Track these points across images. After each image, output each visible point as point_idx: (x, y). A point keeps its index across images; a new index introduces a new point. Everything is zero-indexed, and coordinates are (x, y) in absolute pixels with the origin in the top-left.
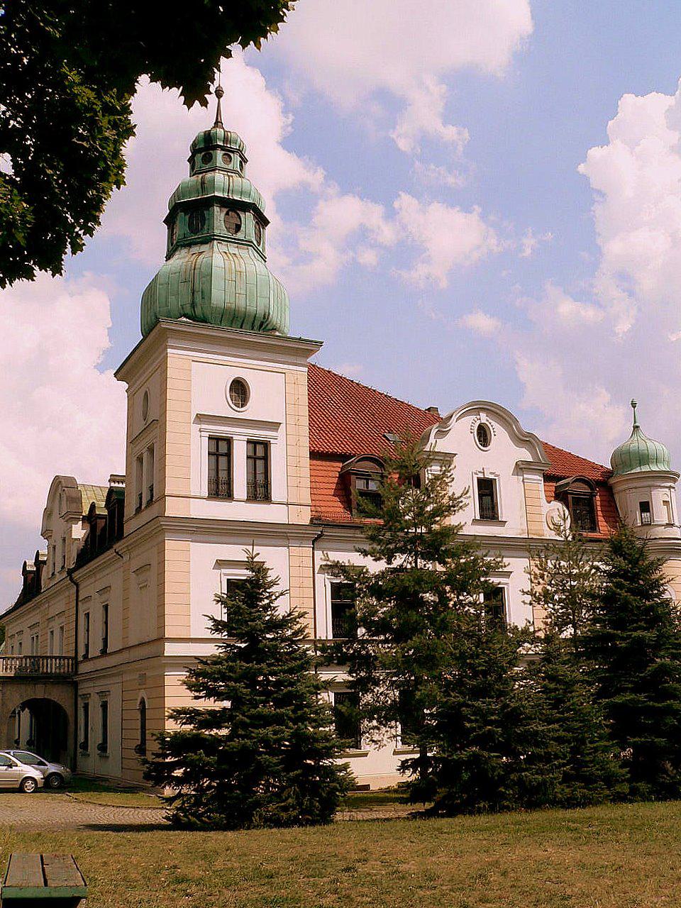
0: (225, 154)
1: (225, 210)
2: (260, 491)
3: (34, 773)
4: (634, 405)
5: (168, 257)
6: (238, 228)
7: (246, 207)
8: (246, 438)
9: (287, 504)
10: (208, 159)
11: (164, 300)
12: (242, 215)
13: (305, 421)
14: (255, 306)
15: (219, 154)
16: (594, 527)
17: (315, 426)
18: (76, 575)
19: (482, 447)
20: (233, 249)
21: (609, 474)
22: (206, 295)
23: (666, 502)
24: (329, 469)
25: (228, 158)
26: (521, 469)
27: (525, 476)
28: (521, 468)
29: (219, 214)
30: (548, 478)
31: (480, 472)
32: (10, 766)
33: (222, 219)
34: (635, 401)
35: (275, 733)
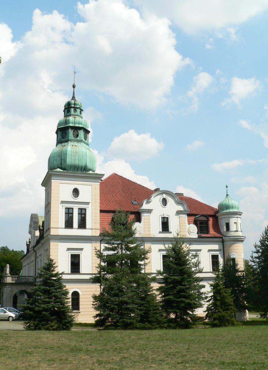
0: (74, 110)
1: (73, 130)
2: (82, 225)
3: (13, 315)
4: (227, 187)
5: (56, 147)
6: (77, 136)
7: (80, 128)
8: (78, 208)
9: (92, 229)
10: (69, 111)
11: (53, 162)
12: (79, 131)
13: (98, 201)
14: (82, 163)
15: (72, 110)
16: (208, 232)
17: (101, 203)
18: (35, 249)
19: (163, 206)
20: (75, 143)
21: (217, 212)
22: (65, 161)
23: (235, 223)
24: (108, 216)
25: (75, 111)
26: (178, 213)
27: (180, 215)
28: (179, 213)
29: (71, 132)
30: (189, 215)
31: (162, 215)
32: (5, 313)
33: (72, 133)
34: (228, 185)
35: (47, 306)
